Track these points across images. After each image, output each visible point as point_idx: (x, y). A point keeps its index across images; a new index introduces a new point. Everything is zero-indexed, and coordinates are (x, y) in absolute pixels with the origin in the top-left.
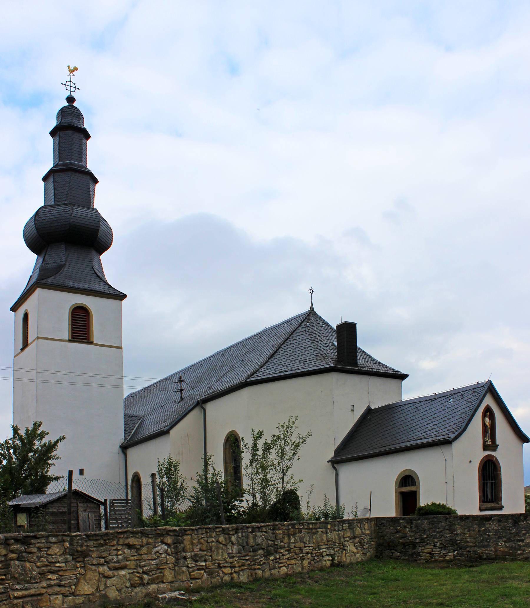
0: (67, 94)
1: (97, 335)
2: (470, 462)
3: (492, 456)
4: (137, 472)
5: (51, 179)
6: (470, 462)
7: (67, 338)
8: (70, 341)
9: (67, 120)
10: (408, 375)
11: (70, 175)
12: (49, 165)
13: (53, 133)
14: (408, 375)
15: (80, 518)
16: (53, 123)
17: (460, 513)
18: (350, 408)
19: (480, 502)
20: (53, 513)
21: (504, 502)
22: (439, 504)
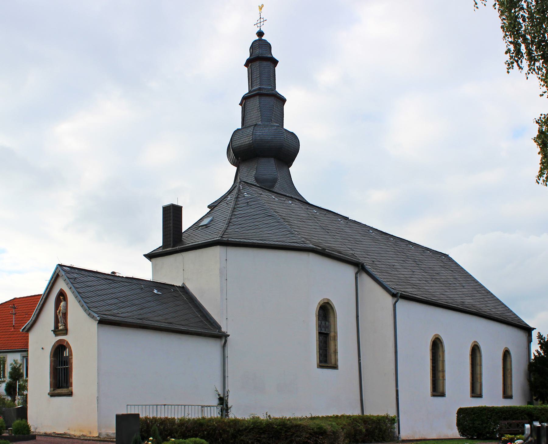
2: (42, 348)
3: (63, 341)
4: (475, 342)
6: (42, 348)
9: (257, 52)
10: (145, 255)
11: (263, 96)
13: (246, 65)
14: (145, 255)
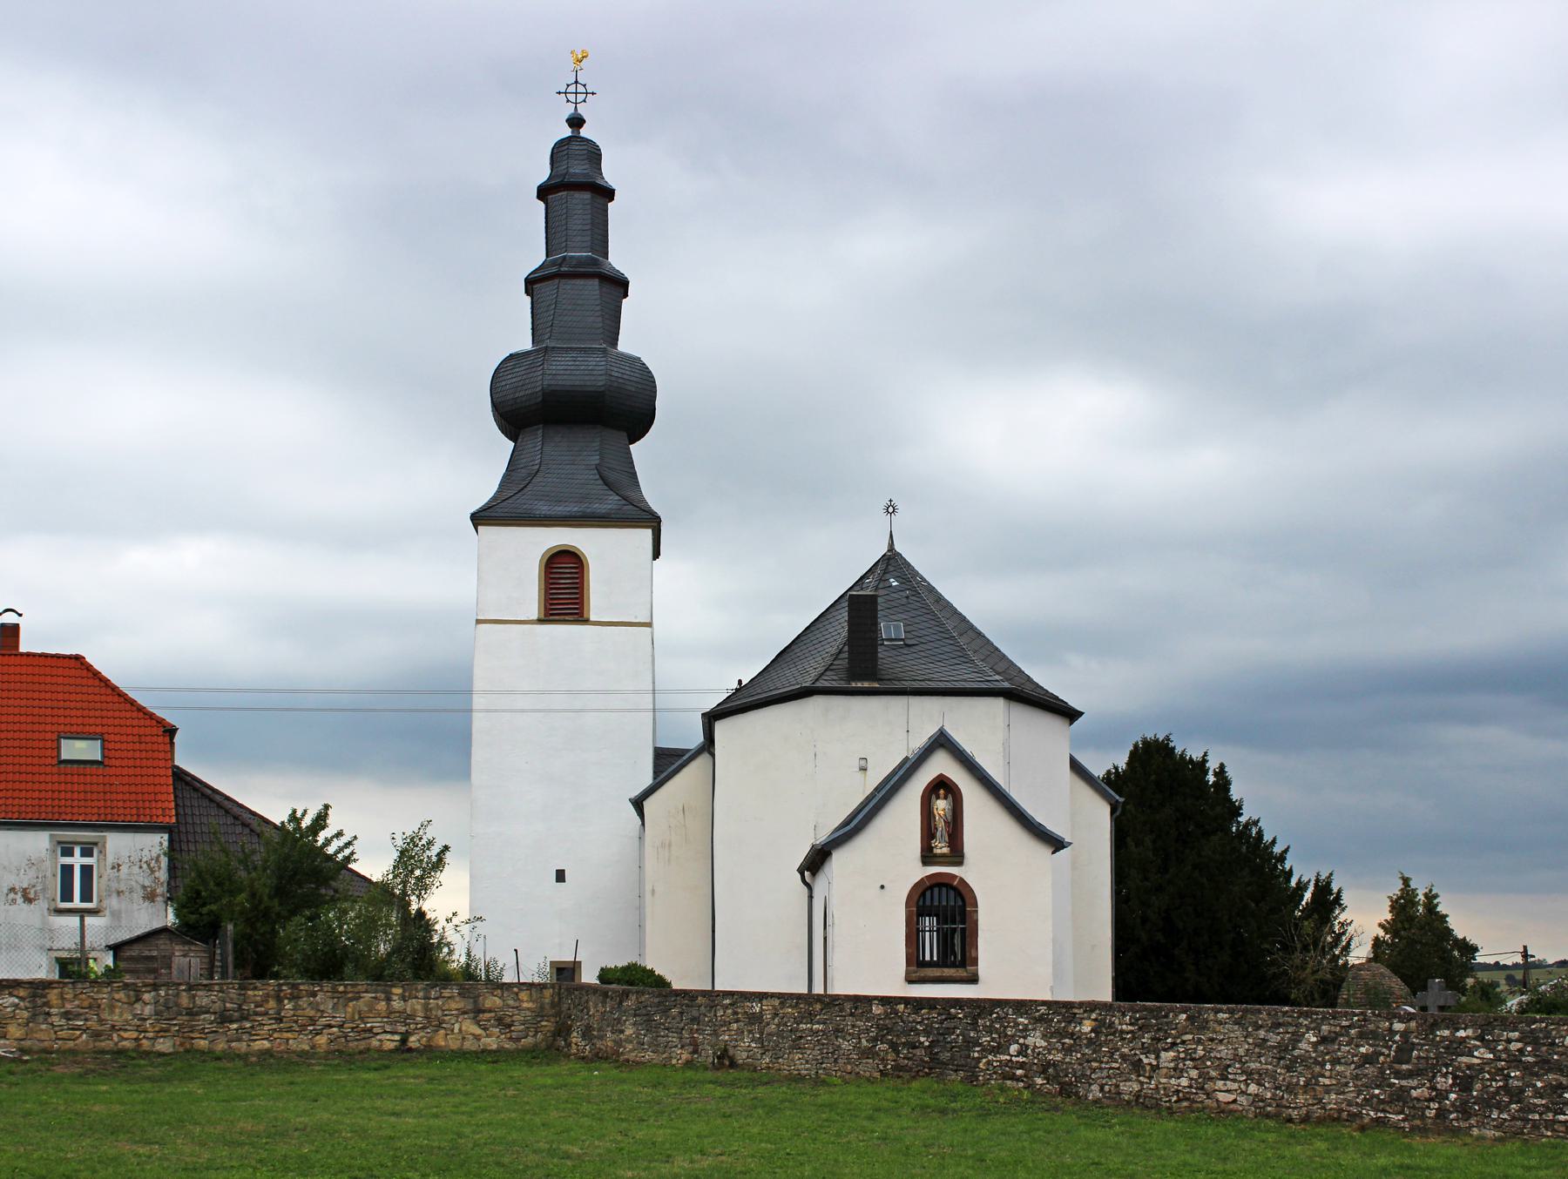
0: (569, 110)
1: (597, 605)
5: (546, 289)
7: (535, 617)
8: (540, 621)
11: (578, 276)
12: (535, 256)
15: (174, 966)
16: (543, 173)
17: (675, 986)
18: (856, 764)
19: (908, 963)
20: (131, 959)
21: (983, 968)
22: (652, 971)
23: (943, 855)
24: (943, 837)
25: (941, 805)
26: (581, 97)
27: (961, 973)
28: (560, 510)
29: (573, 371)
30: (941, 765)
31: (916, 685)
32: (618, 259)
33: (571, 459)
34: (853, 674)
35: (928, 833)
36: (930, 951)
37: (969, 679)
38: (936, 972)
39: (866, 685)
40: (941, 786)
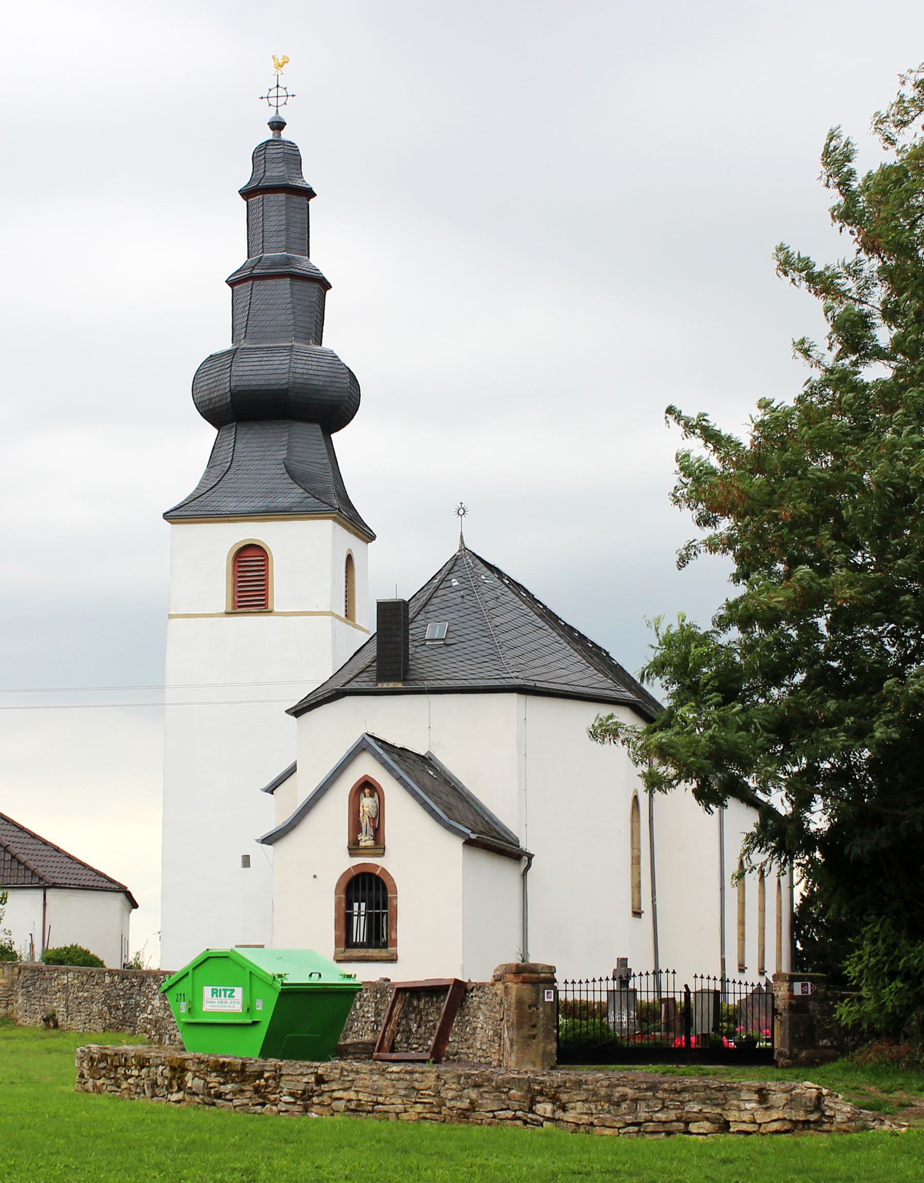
0: (270, 115)
5: (244, 288)
7: (223, 610)
8: (227, 613)
11: (280, 279)
12: (235, 255)
16: (244, 176)
23: (366, 848)
24: (367, 832)
25: (367, 803)
26: (281, 100)
27: (383, 953)
28: (246, 506)
29: (269, 369)
30: (367, 767)
31: (436, 684)
32: (321, 258)
33: (267, 452)
34: (381, 678)
35: (355, 827)
36: (360, 932)
37: (487, 675)
38: (361, 952)
39: (391, 685)
40: (367, 786)
